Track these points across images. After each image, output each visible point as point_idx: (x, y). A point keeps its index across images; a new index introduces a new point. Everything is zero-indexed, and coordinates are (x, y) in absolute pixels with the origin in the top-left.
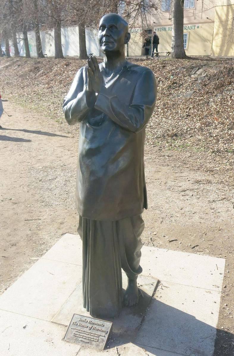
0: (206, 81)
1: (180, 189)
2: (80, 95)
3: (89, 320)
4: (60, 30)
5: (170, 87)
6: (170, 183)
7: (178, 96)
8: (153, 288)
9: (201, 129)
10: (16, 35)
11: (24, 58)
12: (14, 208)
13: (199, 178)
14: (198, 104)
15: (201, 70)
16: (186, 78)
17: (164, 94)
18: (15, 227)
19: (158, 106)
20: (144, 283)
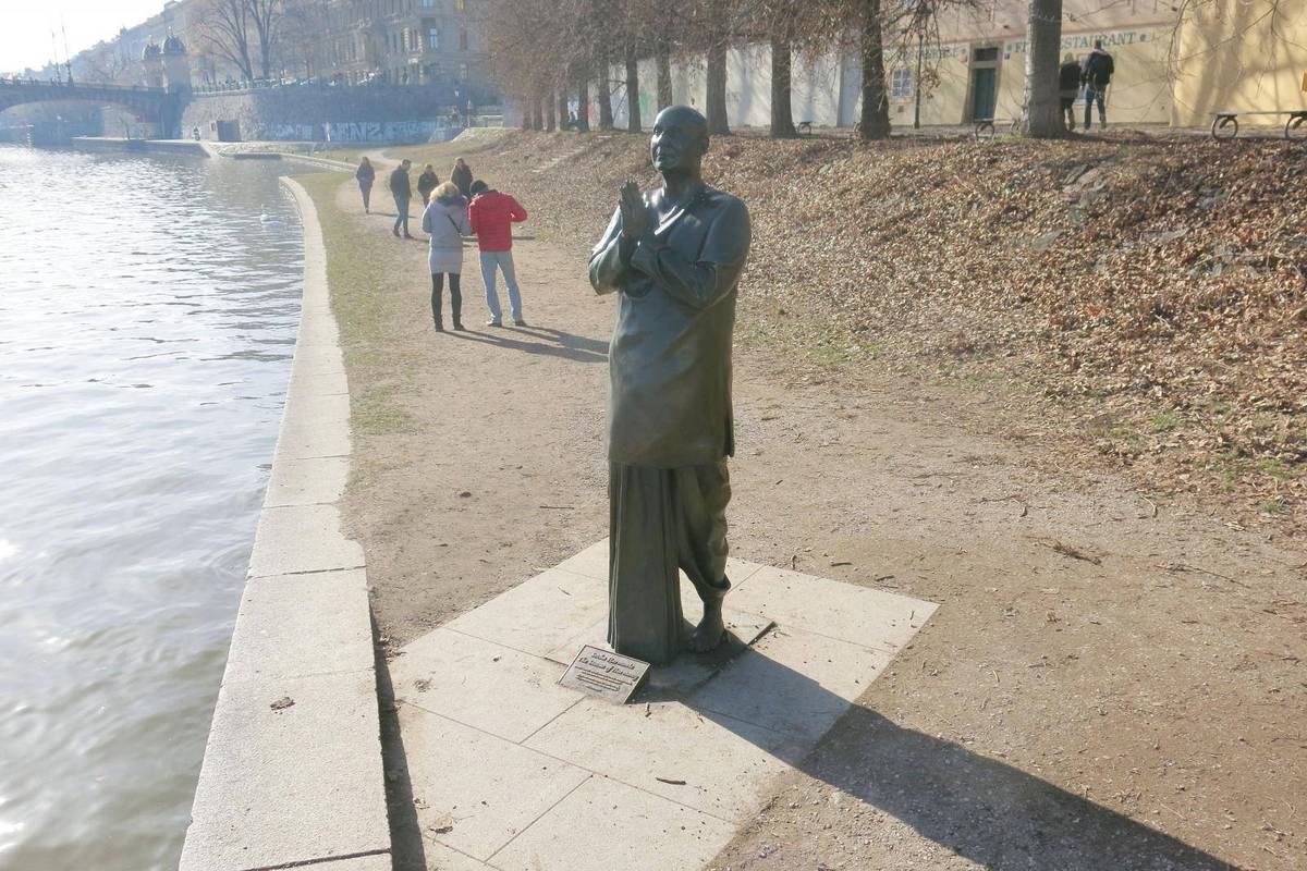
0: (1100, 204)
1: (919, 472)
2: (612, 244)
3: (609, 656)
4: (722, 60)
5: (998, 218)
6: (900, 458)
7: (1015, 246)
8: (756, 632)
9: (1047, 336)
10: (607, 74)
11: (624, 134)
12: (522, 485)
13: (978, 452)
14: (1063, 269)
15: (1092, 173)
16: (1047, 195)
17: (978, 239)
18: (518, 517)
19: (954, 272)
20: (738, 617)
